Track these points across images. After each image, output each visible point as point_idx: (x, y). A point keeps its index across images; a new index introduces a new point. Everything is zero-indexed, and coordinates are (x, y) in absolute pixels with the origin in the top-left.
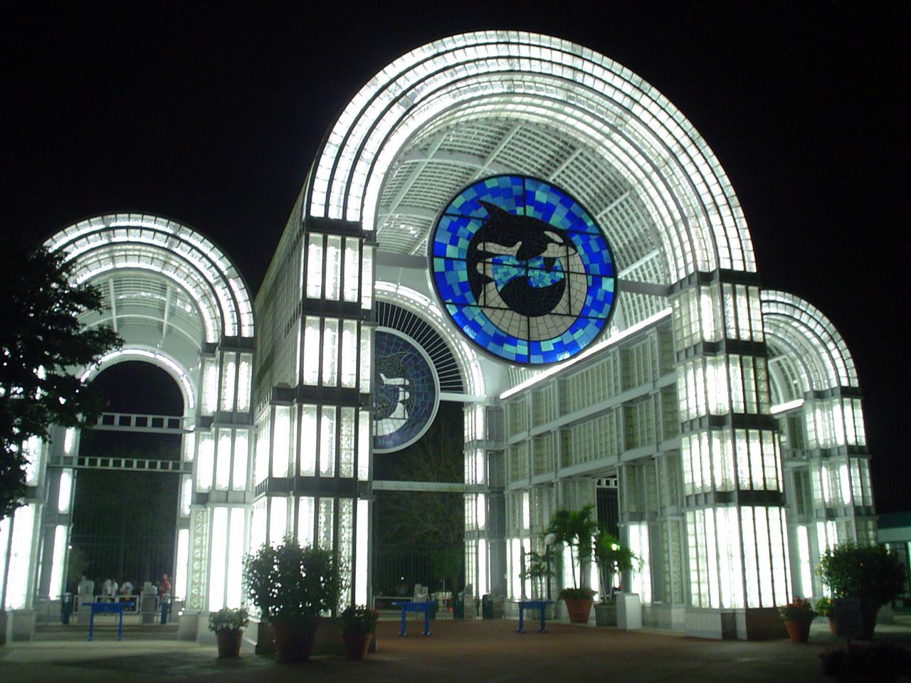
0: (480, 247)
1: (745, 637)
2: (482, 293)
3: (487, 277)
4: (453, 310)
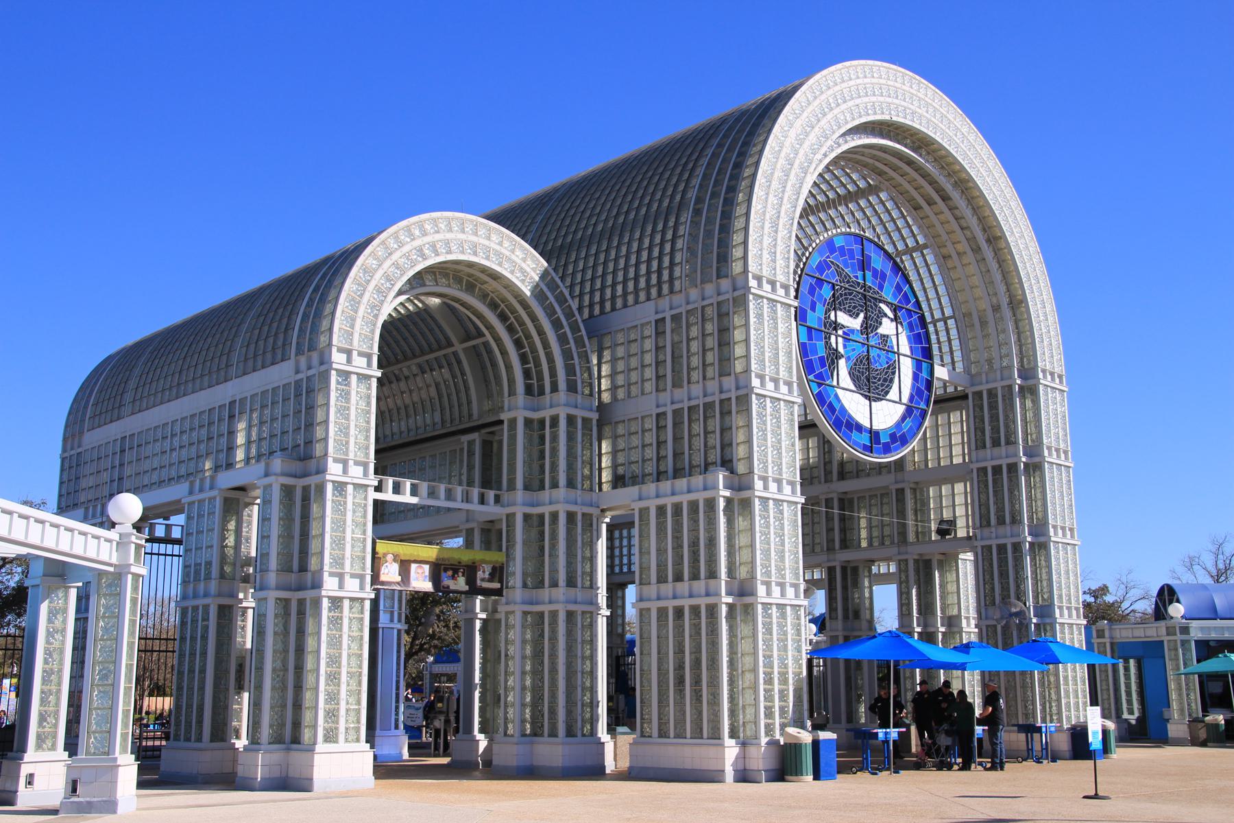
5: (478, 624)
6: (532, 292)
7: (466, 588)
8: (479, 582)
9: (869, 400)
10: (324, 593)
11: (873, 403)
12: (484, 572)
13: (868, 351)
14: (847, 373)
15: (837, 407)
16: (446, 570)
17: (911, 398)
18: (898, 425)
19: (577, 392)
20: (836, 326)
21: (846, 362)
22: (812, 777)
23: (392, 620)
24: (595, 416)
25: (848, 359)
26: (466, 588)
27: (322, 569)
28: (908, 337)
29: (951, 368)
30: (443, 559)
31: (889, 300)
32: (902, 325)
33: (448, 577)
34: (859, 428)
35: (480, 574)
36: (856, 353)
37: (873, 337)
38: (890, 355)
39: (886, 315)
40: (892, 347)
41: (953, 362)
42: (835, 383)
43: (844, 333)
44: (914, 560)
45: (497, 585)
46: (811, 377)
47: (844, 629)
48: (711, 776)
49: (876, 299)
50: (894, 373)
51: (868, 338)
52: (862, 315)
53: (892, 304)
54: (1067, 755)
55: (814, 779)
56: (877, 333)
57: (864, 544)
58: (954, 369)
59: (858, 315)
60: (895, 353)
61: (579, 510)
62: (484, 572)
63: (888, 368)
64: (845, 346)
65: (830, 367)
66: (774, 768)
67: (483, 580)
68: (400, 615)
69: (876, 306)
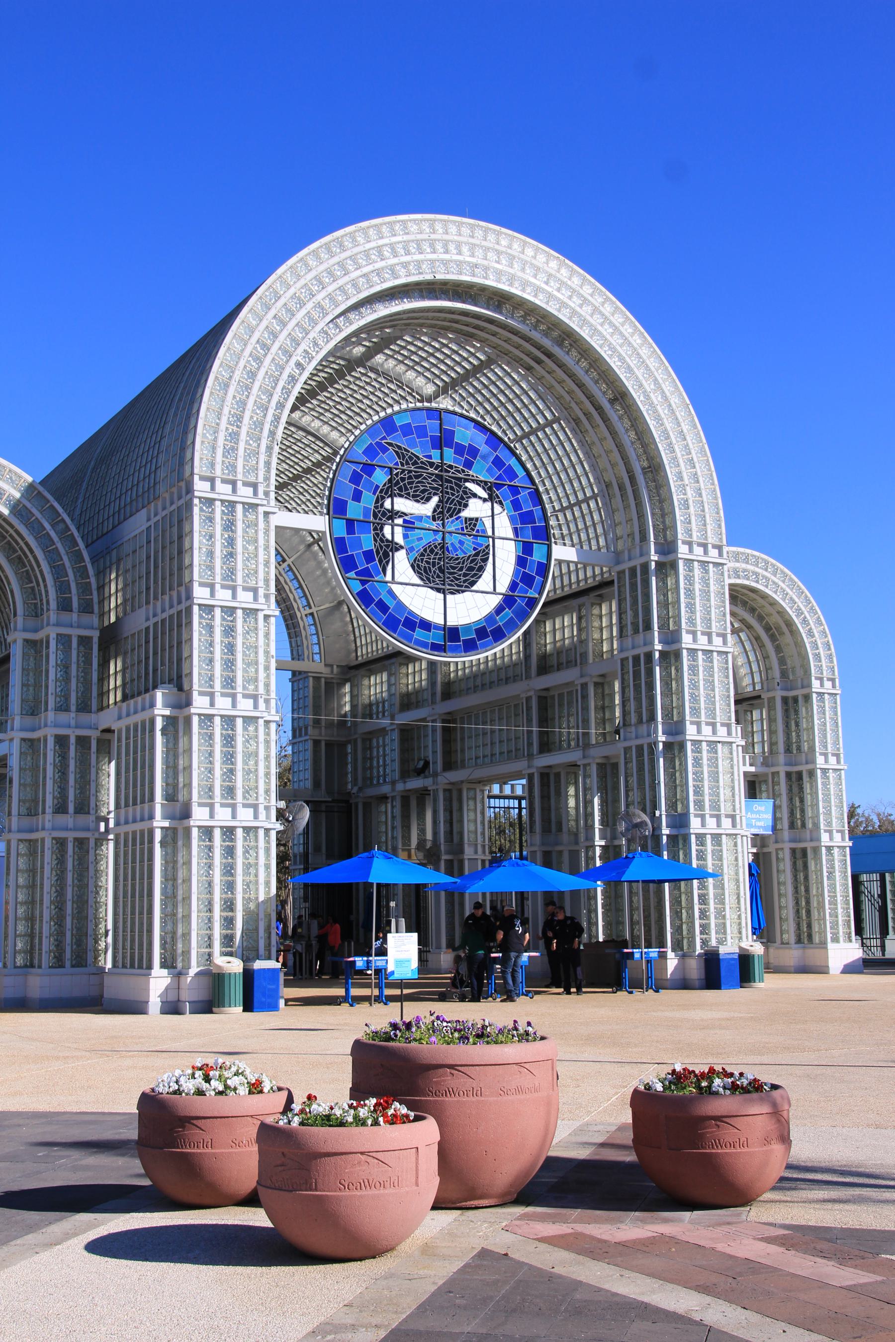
5: (598, 851)
6: (11, 512)
9: (444, 593)
10: (192, 823)
11: (449, 597)
13: (443, 539)
14: (408, 565)
15: (390, 603)
17: (513, 586)
18: (489, 618)
19: (71, 611)
20: (392, 514)
21: (408, 554)
22: (241, 1008)
23: (476, 852)
24: (95, 634)
25: (409, 551)
27: (191, 799)
28: (512, 519)
29: (579, 547)
31: (482, 478)
32: (501, 503)
34: (426, 625)
36: (424, 542)
37: (452, 522)
38: (480, 540)
39: (475, 495)
40: (484, 531)
41: (581, 542)
42: (389, 577)
43: (405, 521)
44: (598, 764)
46: (352, 574)
47: (543, 844)
48: (136, 1008)
49: (460, 479)
50: (485, 560)
51: (443, 525)
52: (435, 500)
53: (486, 483)
54: (697, 983)
55: (244, 1011)
56: (460, 517)
58: (582, 547)
59: (428, 499)
60: (488, 537)
61: (73, 734)
63: (477, 555)
64: (405, 536)
65: (380, 561)
66: (201, 999)
68: (484, 846)
69: (460, 487)
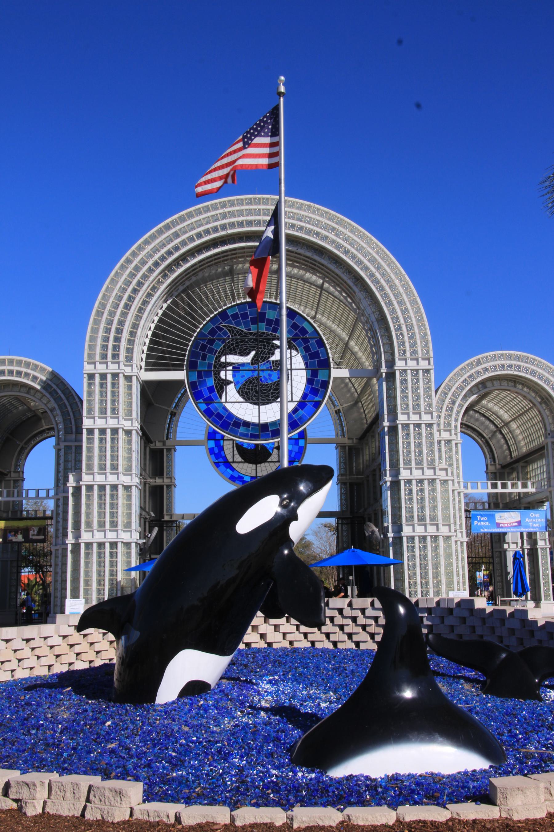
0: (223, 359)
1: (416, 537)
2: (224, 393)
3: (228, 381)
4: (204, 407)
7: (23, 540)
8: (31, 537)
12: (34, 531)
16: (10, 532)
26: (23, 540)
30: (8, 527)
33: (12, 536)
35: (31, 532)
45: (43, 537)
56: (269, 361)
57: (24, 496)
62: (34, 531)
67: (33, 535)
69: (269, 344)
